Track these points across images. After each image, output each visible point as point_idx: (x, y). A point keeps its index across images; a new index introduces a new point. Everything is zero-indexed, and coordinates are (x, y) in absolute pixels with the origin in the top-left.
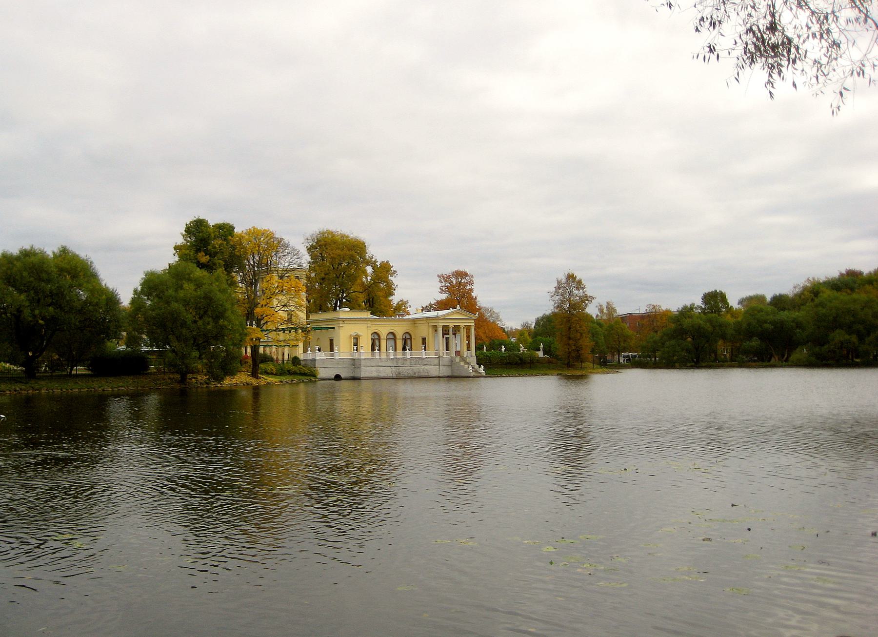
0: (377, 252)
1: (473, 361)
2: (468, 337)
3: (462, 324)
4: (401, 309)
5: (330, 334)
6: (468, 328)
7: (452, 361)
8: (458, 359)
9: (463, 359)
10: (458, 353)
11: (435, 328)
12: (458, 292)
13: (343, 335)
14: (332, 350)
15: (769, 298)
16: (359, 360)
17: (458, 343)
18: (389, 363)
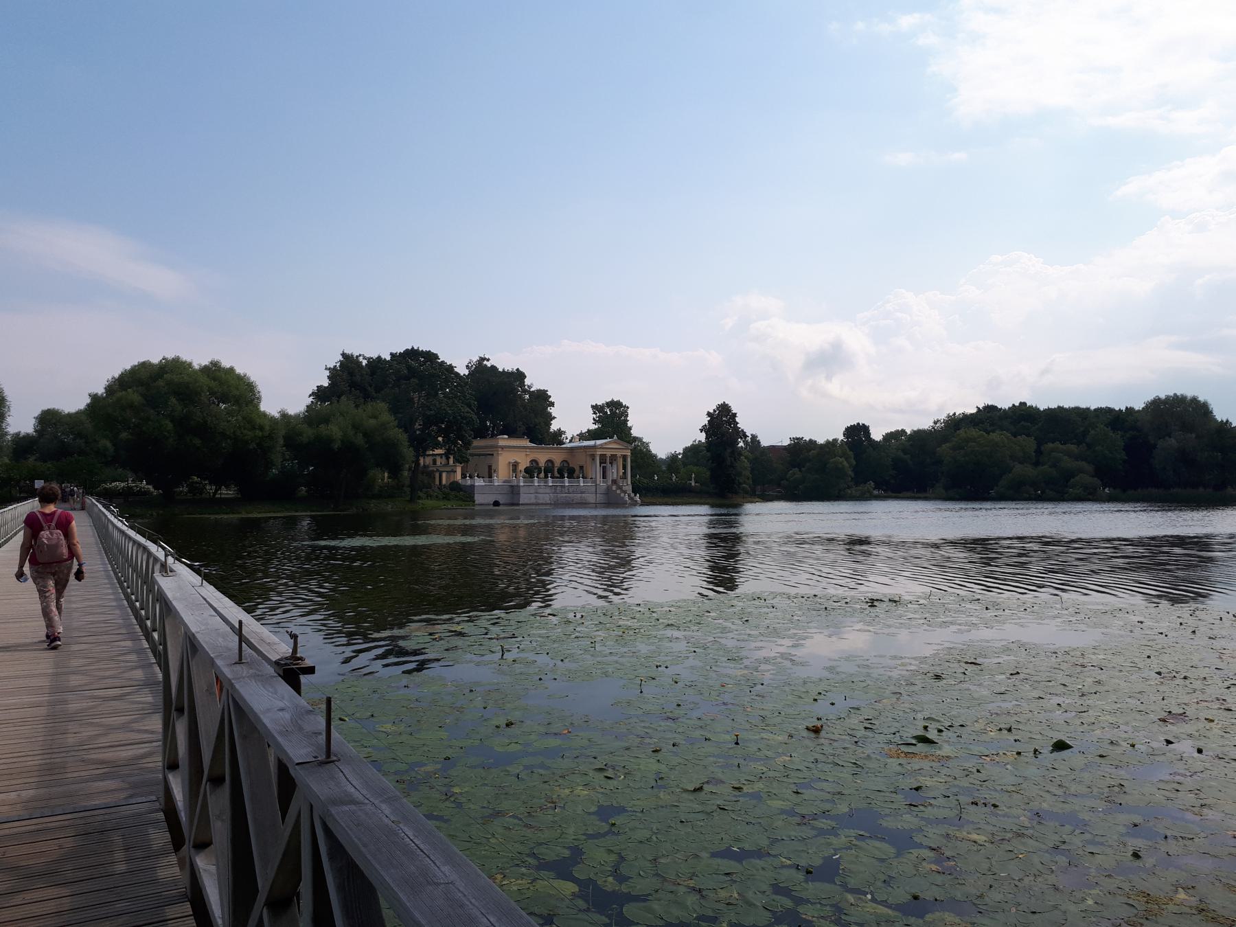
0: (534, 381)
1: (629, 488)
2: (624, 467)
3: (619, 453)
4: (557, 437)
6: (624, 457)
7: (609, 488)
8: (614, 488)
9: (620, 488)
10: (614, 482)
11: (593, 457)
12: (612, 419)
13: (503, 462)
14: (490, 477)
17: (614, 472)
18: (548, 490)
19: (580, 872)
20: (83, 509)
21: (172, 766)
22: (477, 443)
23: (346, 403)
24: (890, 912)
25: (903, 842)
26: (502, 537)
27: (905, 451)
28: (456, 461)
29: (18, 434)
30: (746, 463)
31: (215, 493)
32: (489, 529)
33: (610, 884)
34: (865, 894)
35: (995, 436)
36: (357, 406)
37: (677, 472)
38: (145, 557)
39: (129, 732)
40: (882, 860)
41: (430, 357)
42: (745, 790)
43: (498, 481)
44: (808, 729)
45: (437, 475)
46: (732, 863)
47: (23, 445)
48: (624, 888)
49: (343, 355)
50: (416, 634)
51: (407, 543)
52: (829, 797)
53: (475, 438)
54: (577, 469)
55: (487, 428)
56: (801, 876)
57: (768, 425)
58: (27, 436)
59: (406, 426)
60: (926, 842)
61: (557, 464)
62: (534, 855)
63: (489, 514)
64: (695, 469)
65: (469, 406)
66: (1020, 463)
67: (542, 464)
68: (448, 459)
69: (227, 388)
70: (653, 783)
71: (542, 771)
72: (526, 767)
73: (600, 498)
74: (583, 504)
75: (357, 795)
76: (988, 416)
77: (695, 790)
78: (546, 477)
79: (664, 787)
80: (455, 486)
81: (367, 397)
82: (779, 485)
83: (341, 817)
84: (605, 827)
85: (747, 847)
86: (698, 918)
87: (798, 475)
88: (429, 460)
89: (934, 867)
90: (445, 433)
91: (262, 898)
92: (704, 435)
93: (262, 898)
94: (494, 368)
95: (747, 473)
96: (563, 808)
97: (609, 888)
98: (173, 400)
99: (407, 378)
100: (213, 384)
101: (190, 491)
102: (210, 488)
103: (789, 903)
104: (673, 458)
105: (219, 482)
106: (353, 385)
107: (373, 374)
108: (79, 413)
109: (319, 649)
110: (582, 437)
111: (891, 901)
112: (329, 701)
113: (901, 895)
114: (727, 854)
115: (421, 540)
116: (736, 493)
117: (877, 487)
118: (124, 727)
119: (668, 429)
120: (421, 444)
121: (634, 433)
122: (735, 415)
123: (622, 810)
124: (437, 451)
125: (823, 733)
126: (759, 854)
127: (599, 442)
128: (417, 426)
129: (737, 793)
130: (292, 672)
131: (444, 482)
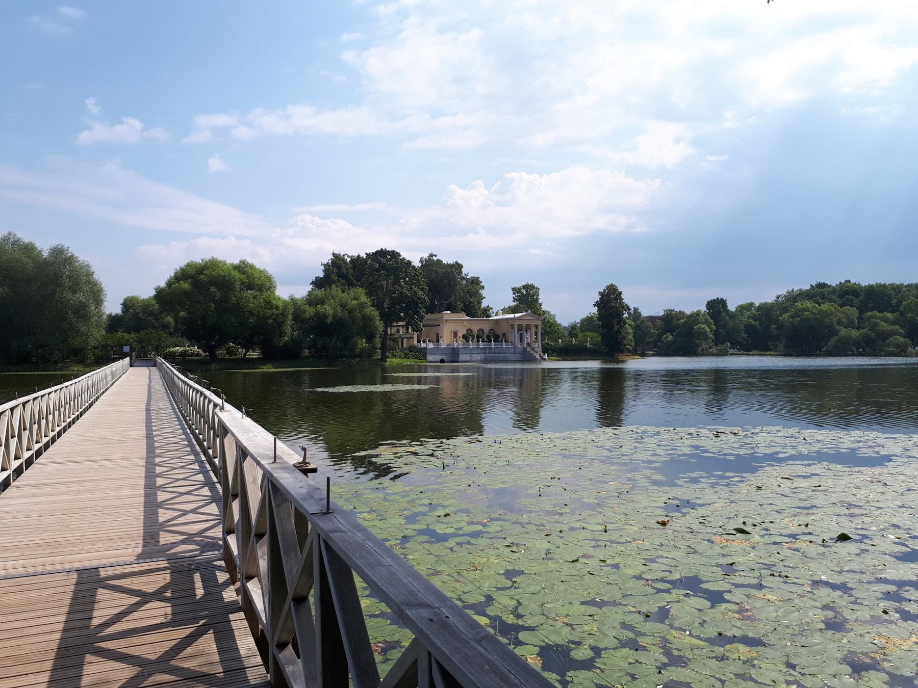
0: (470, 270)
1: (540, 350)
2: (536, 334)
3: (532, 324)
4: (486, 312)
5: (437, 329)
6: (536, 326)
7: (524, 350)
10: (528, 344)
11: (512, 327)
12: (527, 298)
14: (438, 341)
15: (757, 304)
16: (458, 348)
18: (479, 351)
19: (491, 611)
20: (155, 366)
21: (228, 532)
22: (429, 316)
23: (336, 290)
24: (701, 642)
25: (716, 598)
26: (446, 388)
27: (755, 318)
28: (414, 330)
29: (110, 315)
30: (630, 330)
31: (245, 355)
32: (437, 380)
33: (510, 619)
34: (685, 631)
35: (825, 307)
36: (343, 291)
37: (576, 336)
38: (202, 399)
39: (195, 515)
40: (700, 610)
41: (394, 255)
42: (608, 562)
43: (443, 344)
44: (658, 522)
45: (400, 341)
46: (595, 608)
47: (115, 322)
48: (520, 622)
49: (333, 254)
50: (384, 454)
51: (378, 390)
52: (668, 568)
53: (427, 313)
54: (501, 335)
55: (436, 306)
56: (641, 618)
57: (646, 300)
58: (117, 315)
59: (378, 306)
60: (733, 599)
61: (486, 332)
62: (460, 600)
63: (438, 369)
64: (590, 334)
65: (423, 290)
66: (845, 328)
67: (475, 332)
68: (408, 329)
69: (250, 280)
70: (544, 556)
71: (468, 546)
72: (457, 544)
73: (518, 357)
74: (506, 361)
75: (344, 528)
76: (820, 292)
77: (573, 561)
78: (478, 341)
79: (552, 559)
80: (412, 349)
81: (351, 284)
82: (656, 346)
83: (337, 539)
84: (509, 583)
85: (606, 599)
86: (568, 642)
87: (671, 338)
88: (394, 330)
89: (736, 615)
90: (405, 310)
91: (290, 596)
92: (596, 308)
93: (290, 596)
94: (439, 261)
95: (631, 337)
96: (482, 570)
97: (510, 622)
98: (213, 289)
99: (378, 271)
100: (243, 277)
101: (228, 353)
102: (241, 351)
103: (632, 635)
104: (573, 327)
105: (248, 346)
106: (341, 276)
107: (354, 268)
108: (151, 298)
109: (318, 457)
110: (505, 311)
111: (702, 636)
112: (328, 479)
113: (711, 632)
114: (592, 603)
115: (389, 388)
116: (622, 352)
117: (733, 346)
118: (194, 511)
119: (569, 307)
120: (388, 318)
121: (544, 308)
122: (620, 293)
123: (521, 573)
124: (400, 324)
125: (667, 527)
126: (614, 604)
127: (517, 315)
128: (386, 305)
129: (602, 564)
130: (305, 470)
131: (405, 346)
